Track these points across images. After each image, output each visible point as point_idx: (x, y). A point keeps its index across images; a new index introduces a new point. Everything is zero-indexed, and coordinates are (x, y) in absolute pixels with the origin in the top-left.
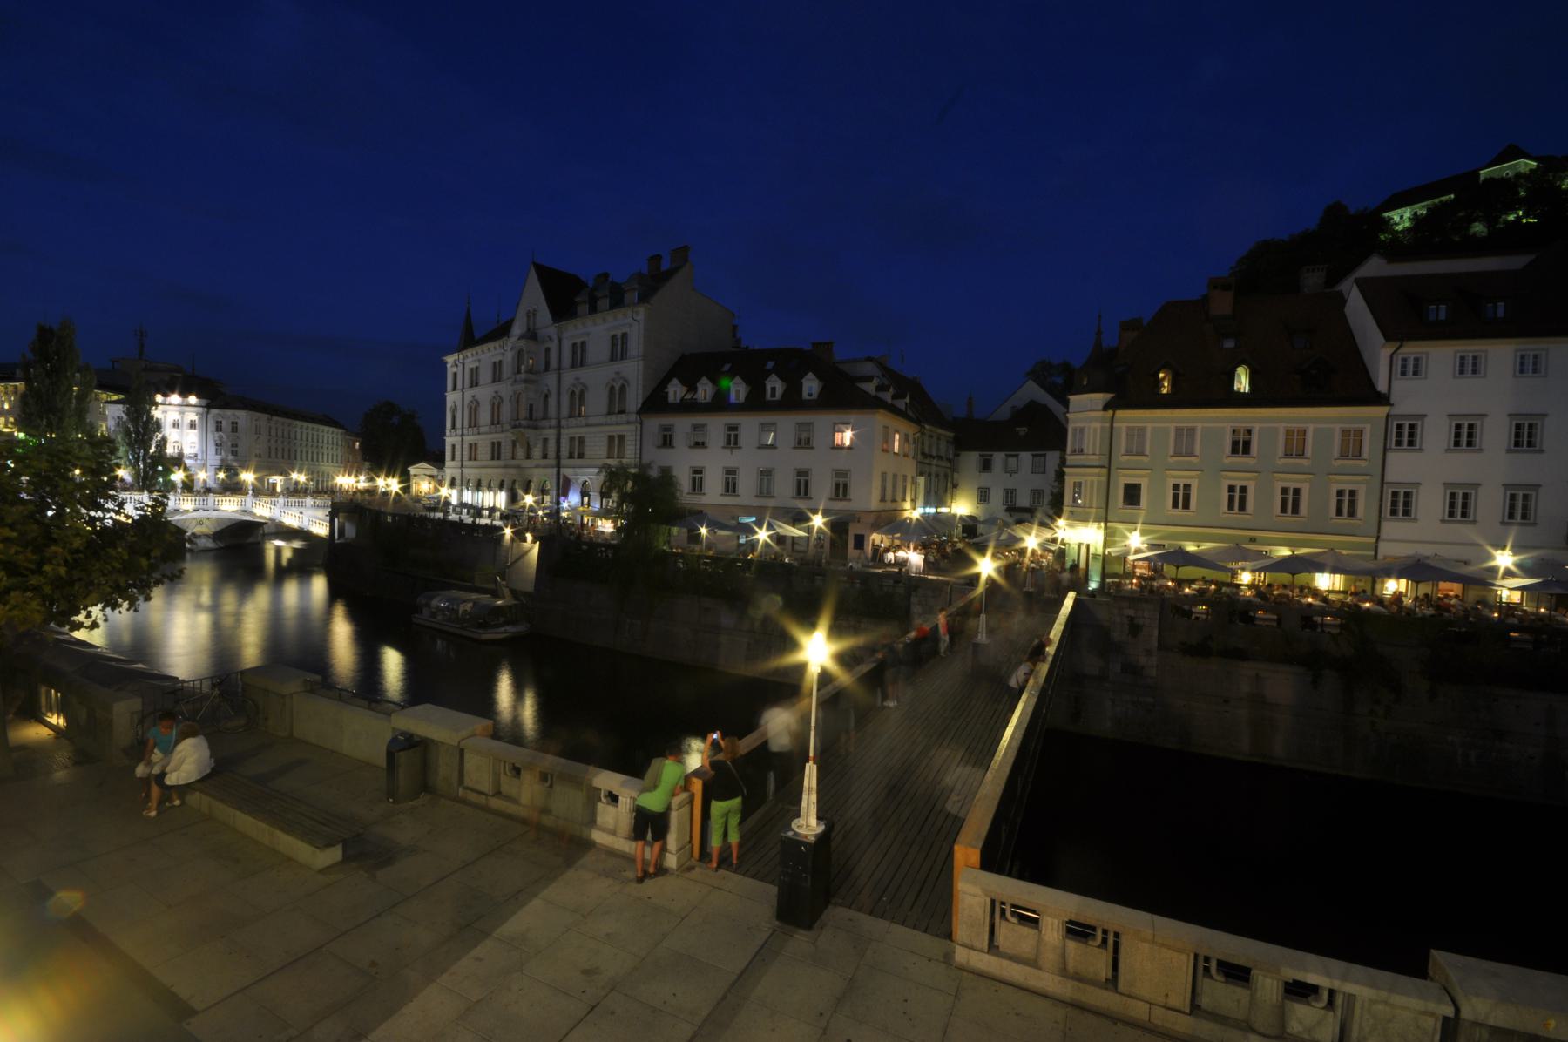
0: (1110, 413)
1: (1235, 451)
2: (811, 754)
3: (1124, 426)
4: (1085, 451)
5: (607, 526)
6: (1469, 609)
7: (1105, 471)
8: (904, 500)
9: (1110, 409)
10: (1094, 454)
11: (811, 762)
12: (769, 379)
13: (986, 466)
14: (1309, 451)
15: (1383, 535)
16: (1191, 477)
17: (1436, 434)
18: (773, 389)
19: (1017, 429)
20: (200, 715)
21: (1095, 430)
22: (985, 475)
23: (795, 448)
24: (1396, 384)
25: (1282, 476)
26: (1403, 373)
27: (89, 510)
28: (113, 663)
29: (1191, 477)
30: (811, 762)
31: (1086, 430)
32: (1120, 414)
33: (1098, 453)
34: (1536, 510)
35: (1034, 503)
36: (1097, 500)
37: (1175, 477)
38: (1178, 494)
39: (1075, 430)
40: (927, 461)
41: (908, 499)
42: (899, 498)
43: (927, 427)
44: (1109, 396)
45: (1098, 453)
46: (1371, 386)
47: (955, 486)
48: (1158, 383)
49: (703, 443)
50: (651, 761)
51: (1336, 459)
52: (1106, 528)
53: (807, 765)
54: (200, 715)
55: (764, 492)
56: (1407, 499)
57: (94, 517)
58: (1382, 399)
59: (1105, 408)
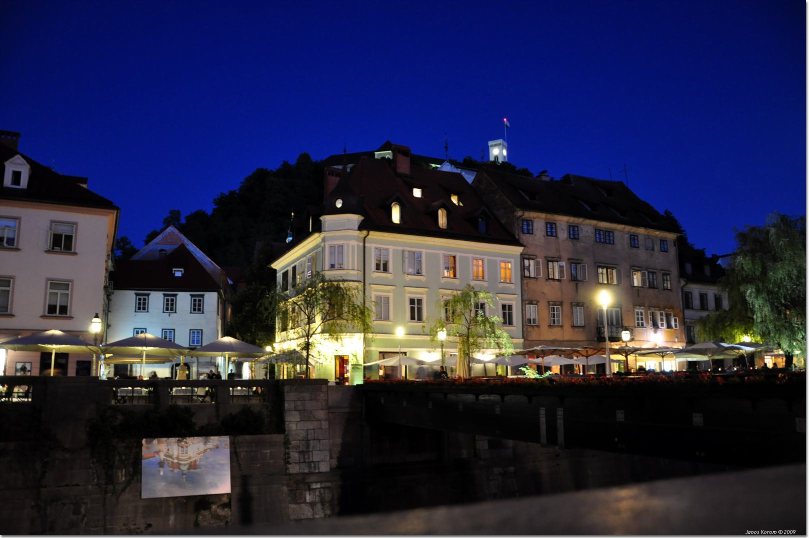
3: (373, 246)
4: (345, 266)
9: (364, 229)
10: (354, 270)
12: (11, 160)
14: (424, 272)
16: (389, 292)
18: (17, 176)
19: (174, 269)
21: (353, 247)
22: (142, 315)
27: (181, 387)
29: (389, 292)
31: (345, 248)
33: (356, 269)
35: (193, 342)
37: (410, 293)
38: (414, 307)
45: (356, 269)
49: (11, 241)
57: (5, 398)
59: (361, 228)
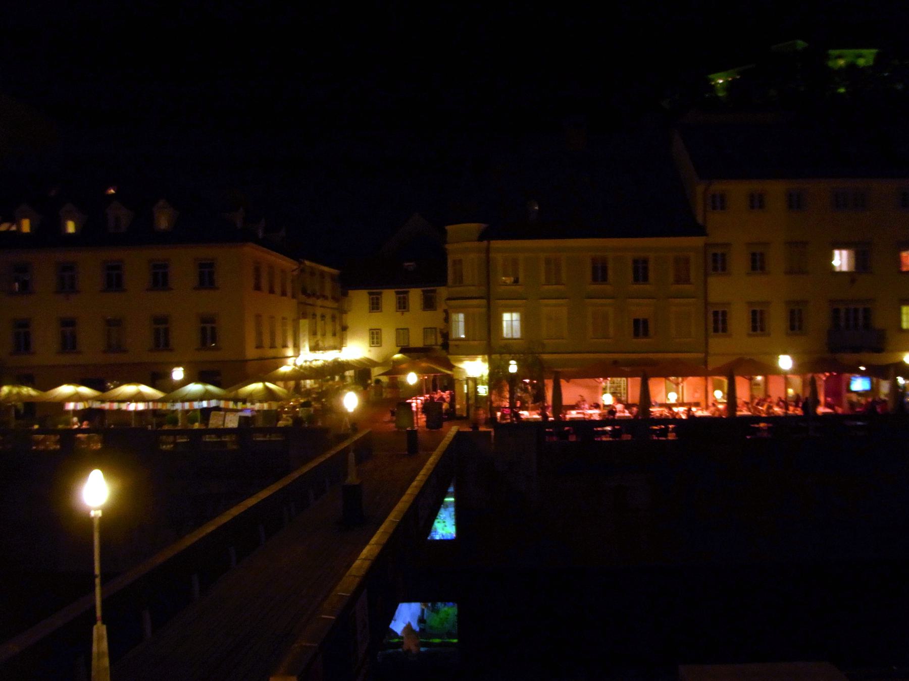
0: (485, 243)
1: (595, 279)
2: (99, 613)
5: (785, 362)
6: (764, 402)
7: (484, 302)
8: (285, 346)
11: (99, 623)
13: (375, 306)
17: (739, 262)
20: (331, 617)
22: (376, 315)
23: (195, 289)
25: (546, 301)
26: (714, 208)
30: (99, 623)
32: (496, 244)
34: (706, 324)
39: (455, 262)
40: (310, 301)
41: (290, 344)
42: (279, 341)
43: (307, 263)
44: (483, 226)
47: (344, 329)
50: (398, 605)
53: (95, 627)
54: (331, 617)
55: (69, 344)
58: (699, 230)
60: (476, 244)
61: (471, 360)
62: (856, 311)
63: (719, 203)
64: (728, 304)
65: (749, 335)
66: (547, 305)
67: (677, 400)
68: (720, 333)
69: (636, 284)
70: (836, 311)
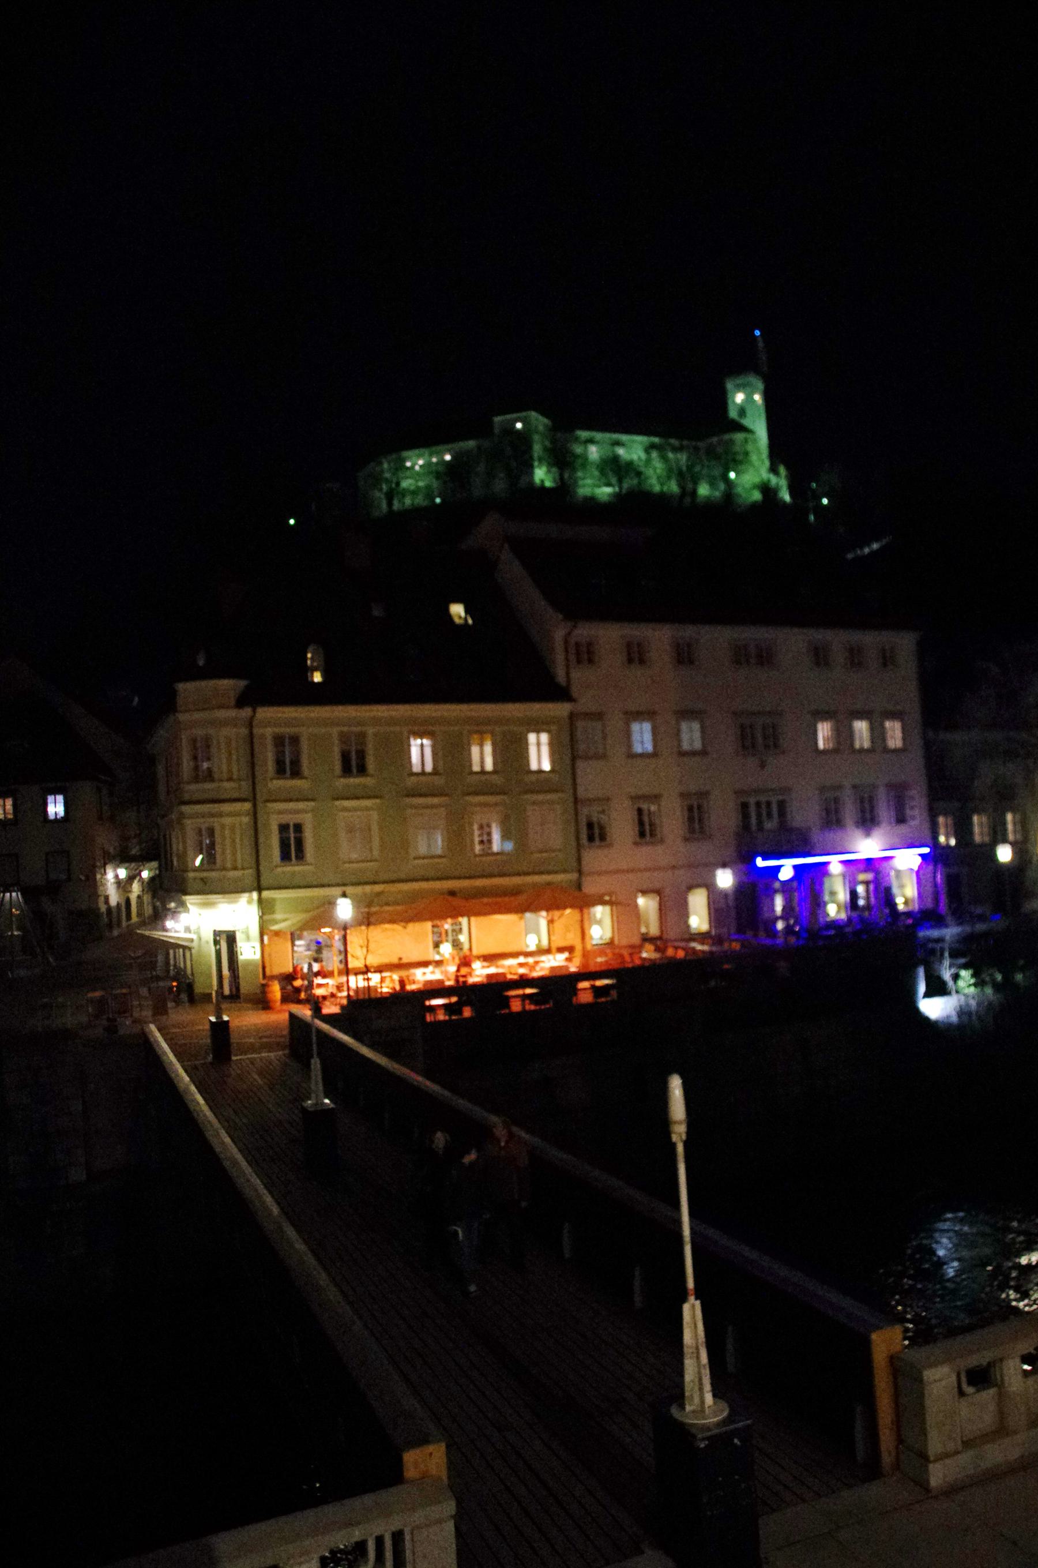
0: (247, 712)
1: (347, 770)
2: (691, 1284)
4: (216, 776)
7: (247, 806)
15: (585, 869)
24: (575, 674)
25: (347, 803)
26: (579, 662)
28: (859, 1426)
32: (265, 713)
36: (244, 854)
37: (280, 812)
44: (242, 683)
46: (549, 677)
48: (305, 671)
51: (272, 779)
52: (260, 901)
56: (298, 835)
58: (562, 694)
60: (232, 713)
61: (229, 903)
62: (769, 804)
63: (585, 654)
64: (787, 790)
65: (636, 844)
66: (345, 809)
67: (538, 946)
68: (597, 842)
69: (278, 779)
70: (745, 806)
